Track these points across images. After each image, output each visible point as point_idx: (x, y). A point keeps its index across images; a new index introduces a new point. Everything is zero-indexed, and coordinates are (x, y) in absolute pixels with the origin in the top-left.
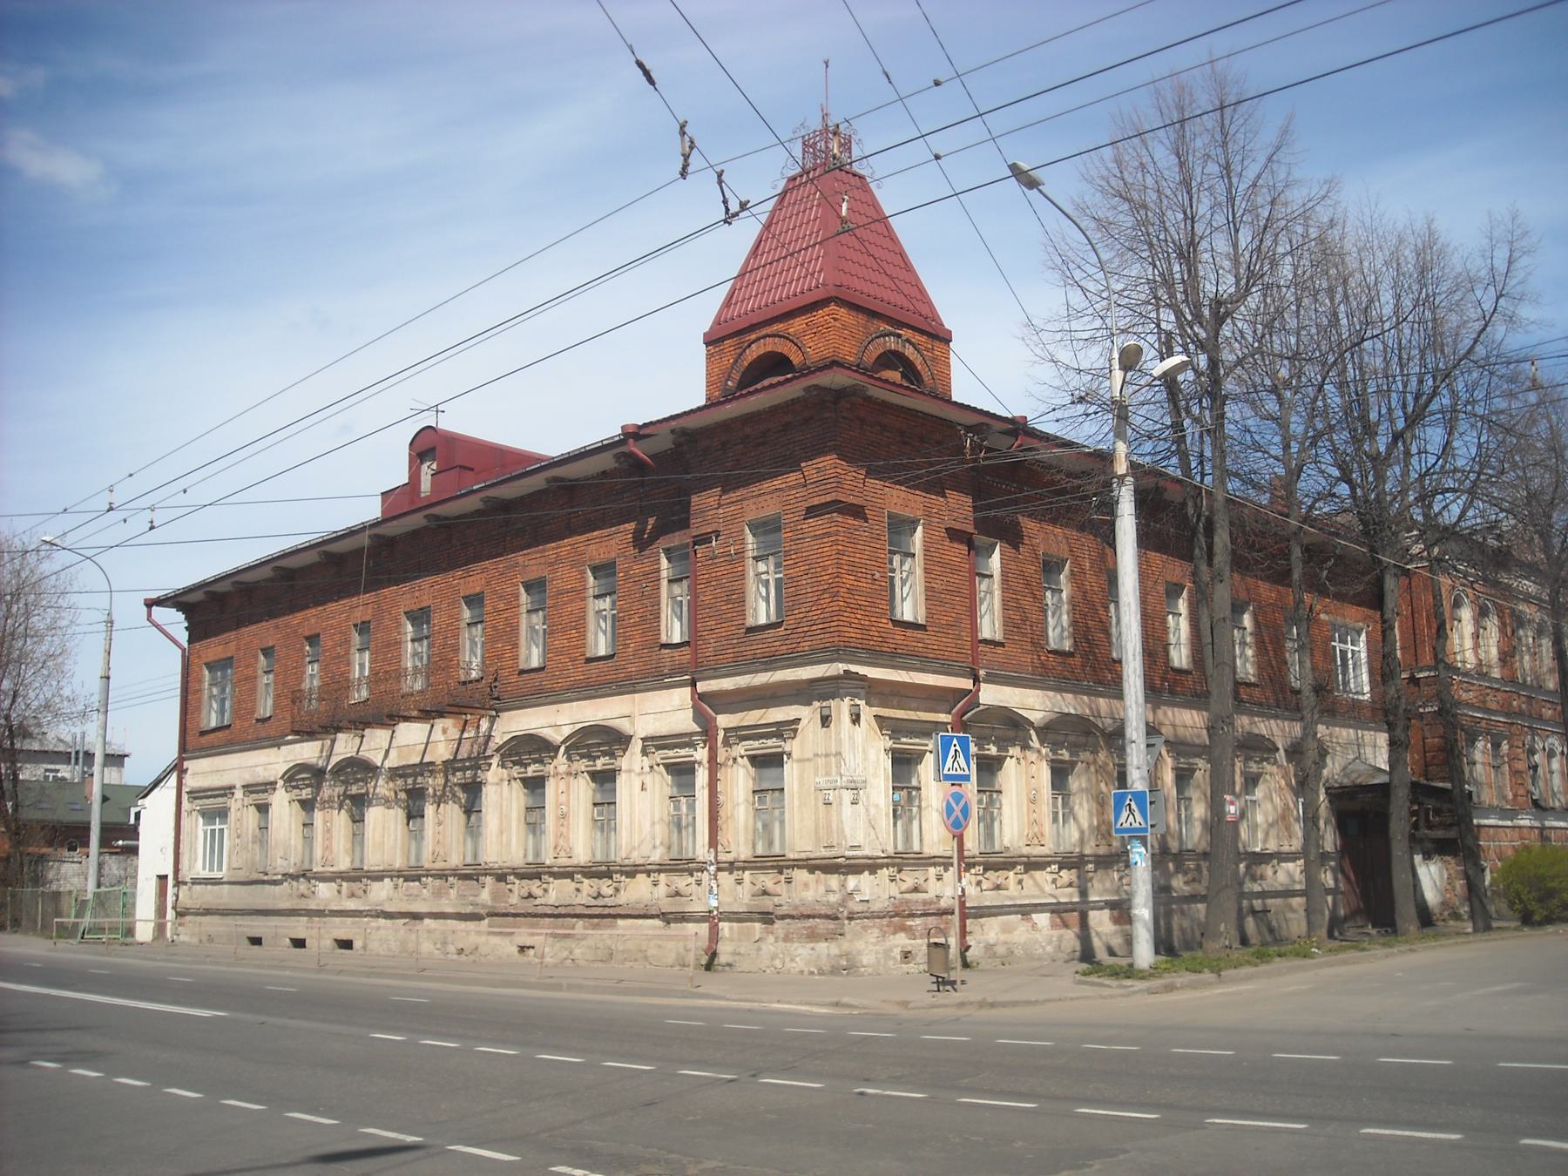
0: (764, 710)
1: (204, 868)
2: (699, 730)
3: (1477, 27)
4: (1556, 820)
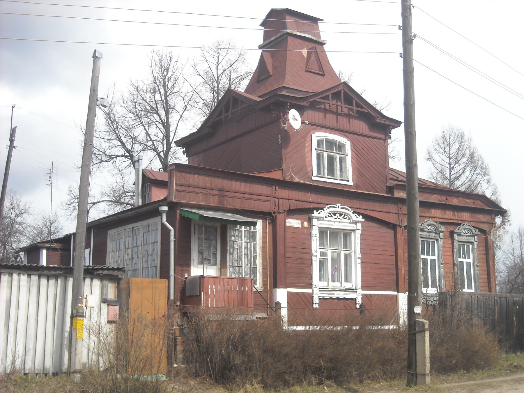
0: (121, 145)
1: (322, 290)
2: (405, 177)
3: (374, 211)
4: (302, 20)
